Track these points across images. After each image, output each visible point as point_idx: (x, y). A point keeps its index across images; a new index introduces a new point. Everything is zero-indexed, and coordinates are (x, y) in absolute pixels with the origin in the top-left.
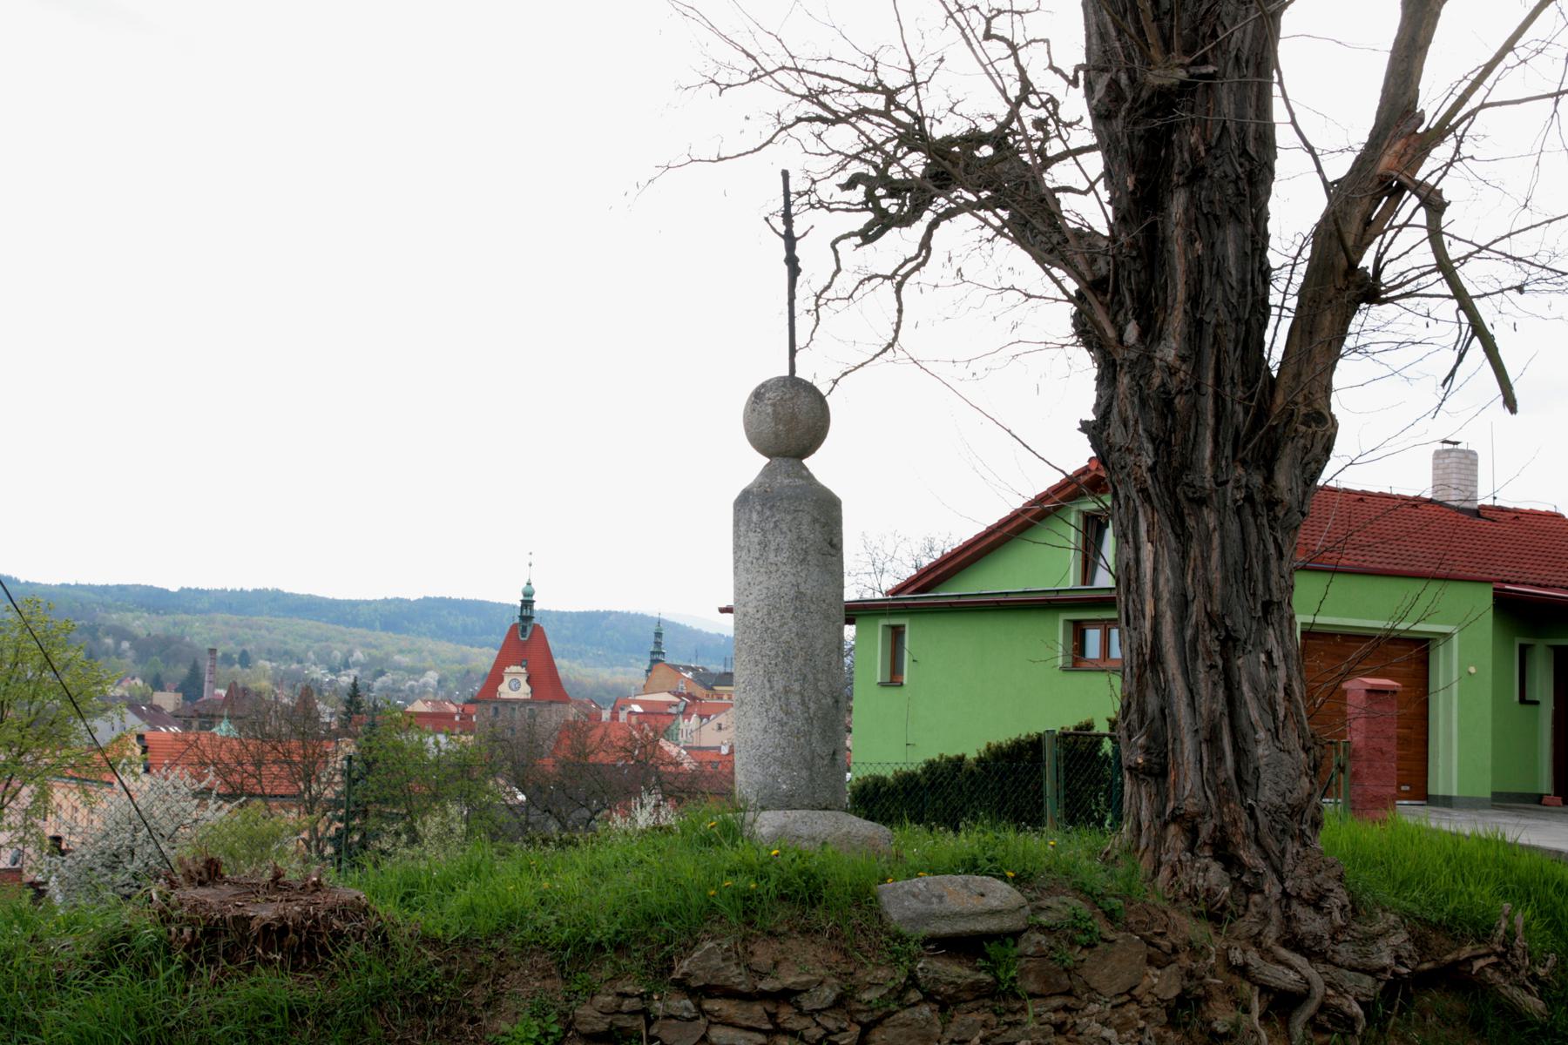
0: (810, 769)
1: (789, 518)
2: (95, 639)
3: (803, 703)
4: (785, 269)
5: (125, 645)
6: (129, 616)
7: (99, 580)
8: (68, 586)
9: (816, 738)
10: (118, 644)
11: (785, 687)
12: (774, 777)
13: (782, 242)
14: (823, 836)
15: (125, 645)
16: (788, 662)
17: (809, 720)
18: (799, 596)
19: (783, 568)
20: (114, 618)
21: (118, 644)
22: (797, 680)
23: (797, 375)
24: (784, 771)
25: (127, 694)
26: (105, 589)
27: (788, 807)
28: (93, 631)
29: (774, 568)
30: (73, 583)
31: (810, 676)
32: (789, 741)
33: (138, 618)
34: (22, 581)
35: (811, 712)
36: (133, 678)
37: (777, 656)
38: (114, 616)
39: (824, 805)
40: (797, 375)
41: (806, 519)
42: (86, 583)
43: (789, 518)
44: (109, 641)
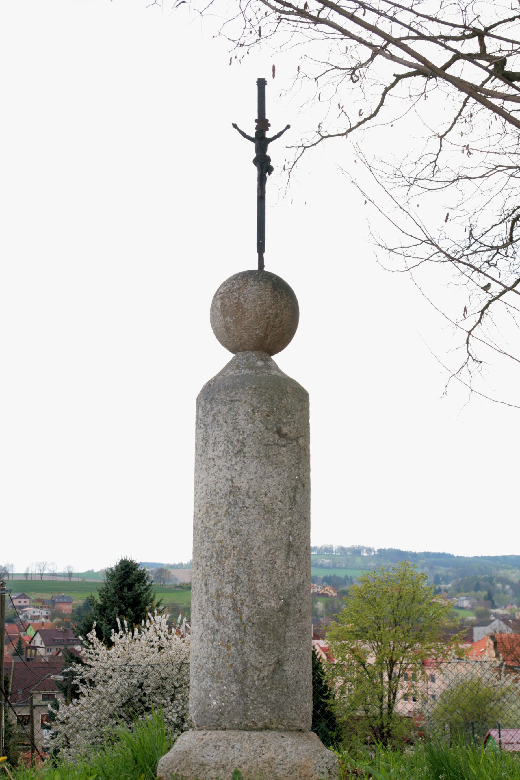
0: (241, 682)
1: (225, 409)
2: (492, 584)
3: (235, 607)
4: (254, 171)
5: (507, 587)
6: (509, 572)
7: (493, 554)
8: (478, 557)
9: (249, 646)
10: (504, 587)
11: (217, 590)
12: (206, 691)
13: (252, 146)
14: (236, 763)
15: (507, 587)
16: (220, 562)
17: (241, 627)
18: (234, 491)
19: (220, 463)
20: (502, 573)
21: (504, 587)
22: (229, 583)
23: (265, 269)
24: (215, 685)
25: (509, 613)
26: (496, 558)
27: (218, 727)
28: (490, 580)
29: (212, 463)
30: (480, 556)
31: (244, 578)
32: (220, 650)
33: (514, 573)
34: (456, 556)
35: (244, 617)
36: (512, 605)
37: (212, 557)
38: (501, 572)
39: (260, 725)
40: (265, 269)
41: (243, 408)
42: (487, 555)
43: (225, 409)
44: (499, 585)
